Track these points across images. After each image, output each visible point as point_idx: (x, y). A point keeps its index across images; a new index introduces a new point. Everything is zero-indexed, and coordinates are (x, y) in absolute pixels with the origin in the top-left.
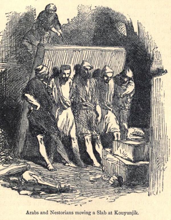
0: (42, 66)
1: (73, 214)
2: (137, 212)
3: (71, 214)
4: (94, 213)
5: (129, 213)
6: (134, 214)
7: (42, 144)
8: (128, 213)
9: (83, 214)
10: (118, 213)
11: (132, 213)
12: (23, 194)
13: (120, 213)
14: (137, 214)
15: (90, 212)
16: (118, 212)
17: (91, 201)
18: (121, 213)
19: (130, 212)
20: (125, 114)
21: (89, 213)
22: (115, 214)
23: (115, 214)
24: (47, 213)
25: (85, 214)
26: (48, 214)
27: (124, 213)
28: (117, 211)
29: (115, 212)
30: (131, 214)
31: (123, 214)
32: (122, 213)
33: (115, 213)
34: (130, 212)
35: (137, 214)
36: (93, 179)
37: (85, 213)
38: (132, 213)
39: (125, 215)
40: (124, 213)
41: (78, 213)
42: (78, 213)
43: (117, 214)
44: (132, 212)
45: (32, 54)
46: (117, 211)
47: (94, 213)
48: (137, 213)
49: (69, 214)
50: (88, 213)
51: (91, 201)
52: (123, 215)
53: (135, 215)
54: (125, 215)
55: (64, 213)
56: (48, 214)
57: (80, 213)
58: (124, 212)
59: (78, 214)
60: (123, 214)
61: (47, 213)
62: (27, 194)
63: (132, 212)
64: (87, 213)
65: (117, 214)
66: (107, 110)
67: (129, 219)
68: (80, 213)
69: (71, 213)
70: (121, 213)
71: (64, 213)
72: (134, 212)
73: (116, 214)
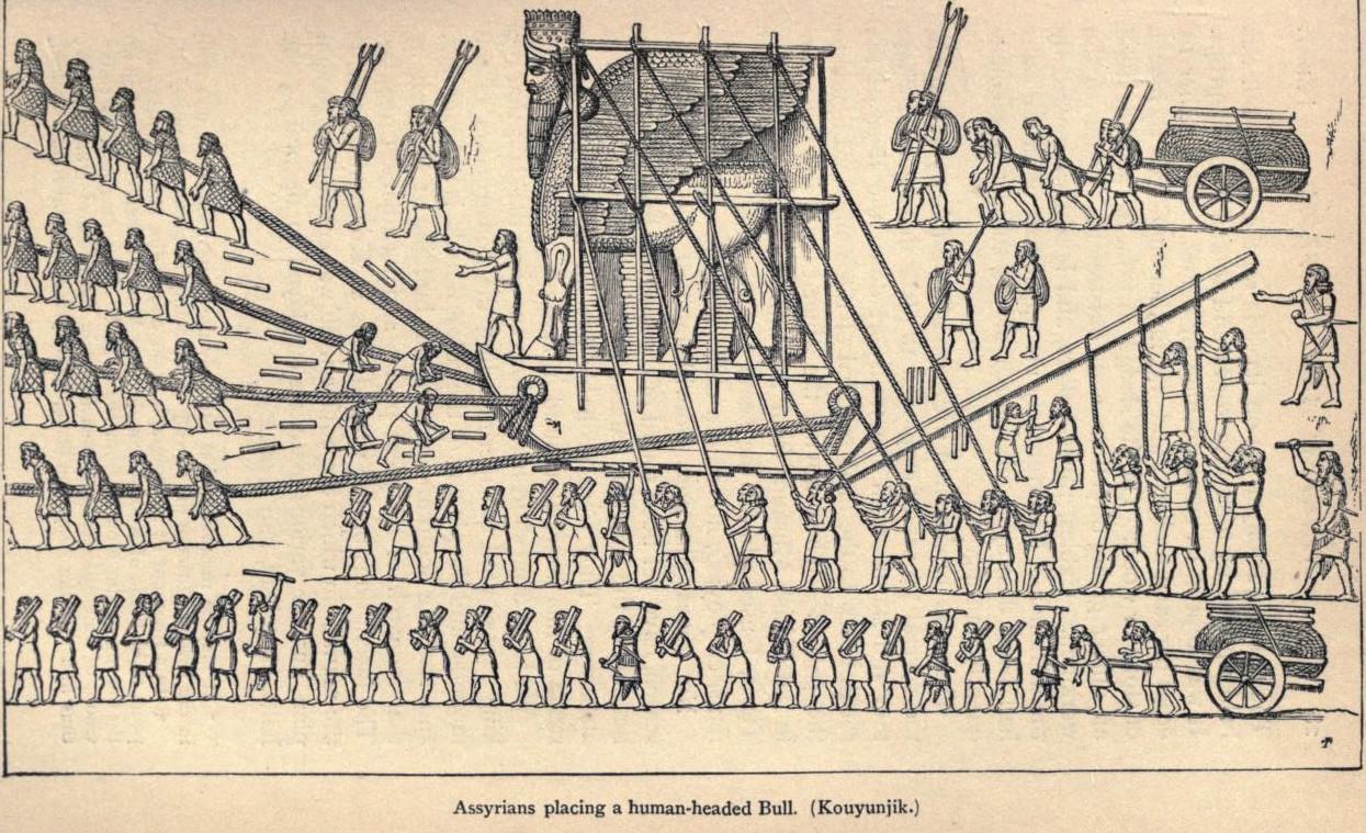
0: (228, 642)
1: (533, 811)
4: (617, 810)
10: (831, 809)
13: (838, 810)
15: (603, 807)
16: (830, 807)
17: (1158, 272)
18: (838, 809)
20: (938, 285)
21: (600, 812)
22: (821, 812)
24: (726, 811)
26: (749, 813)
27: (855, 809)
36: (809, 258)
40: (855, 809)
44: (886, 804)
45: (81, 91)
47: (617, 810)
51: (1158, 272)
52: (852, 817)
55: (501, 810)
56: (547, 807)
57: (838, 810)
58: (857, 806)
61: (726, 811)
63: (886, 804)
65: (829, 812)
70: (838, 809)
71: (501, 810)
72: (892, 803)
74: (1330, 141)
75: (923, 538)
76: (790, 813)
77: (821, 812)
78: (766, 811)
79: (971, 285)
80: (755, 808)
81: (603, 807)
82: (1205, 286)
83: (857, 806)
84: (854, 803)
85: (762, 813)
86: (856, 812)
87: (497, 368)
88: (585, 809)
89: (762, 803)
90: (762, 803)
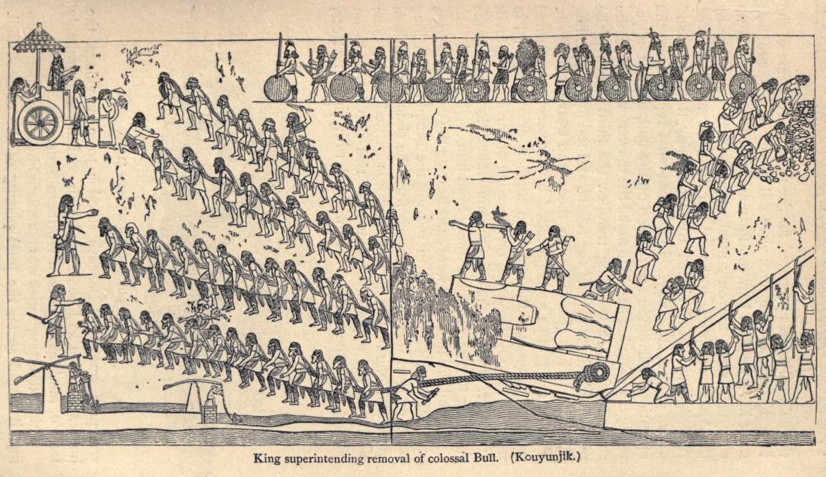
2: (571, 455)
3: (291, 458)
5: (552, 458)
6: (564, 459)
7: (263, 306)
8: (549, 458)
9: (397, 461)
10: (263, 460)
11: (559, 458)
12: (643, 36)
14: (571, 459)
15: (279, 458)
16: (262, 458)
19: (554, 456)
22: (256, 462)
23: (256, 462)
24: (344, 460)
25: (315, 461)
27: (538, 457)
28: (522, 453)
29: (254, 456)
30: (557, 459)
31: (537, 460)
32: (535, 458)
33: (254, 460)
34: (554, 456)
35: (571, 459)
37: (317, 459)
38: (559, 458)
39: (540, 463)
41: (384, 460)
42: (384, 460)
43: (522, 460)
46: (522, 453)
48: (572, 457)
49: (383, 462)
50: (274, 460)
53: (566, 461)
54: (540, 463)
55: (313, 460)
57: (391, 460)
58: (540, 456)
59: (386, 462)
60: (537, 460)
62: (703, 219)
64: (271, 459)
66: (58, 324)
67: (537, 475)
68: (391, 460)
69: (290, 459)
72: (562, 453)
73: (258, 460)
74: (511, 149)
75: (240, 300)
76: (494, 461)
77: (517, 460)
78: (478, 459)
79: (59, 217)
80: (365, 461)
81: (279, 458)
82: (775, 278)
83: (540, 456)
84: (538, 454)
85: (476, 461)
86: (539, 460)
87: (610, 382)
88: (353, 460)
89: (476, 454)
90: (476, 454)
